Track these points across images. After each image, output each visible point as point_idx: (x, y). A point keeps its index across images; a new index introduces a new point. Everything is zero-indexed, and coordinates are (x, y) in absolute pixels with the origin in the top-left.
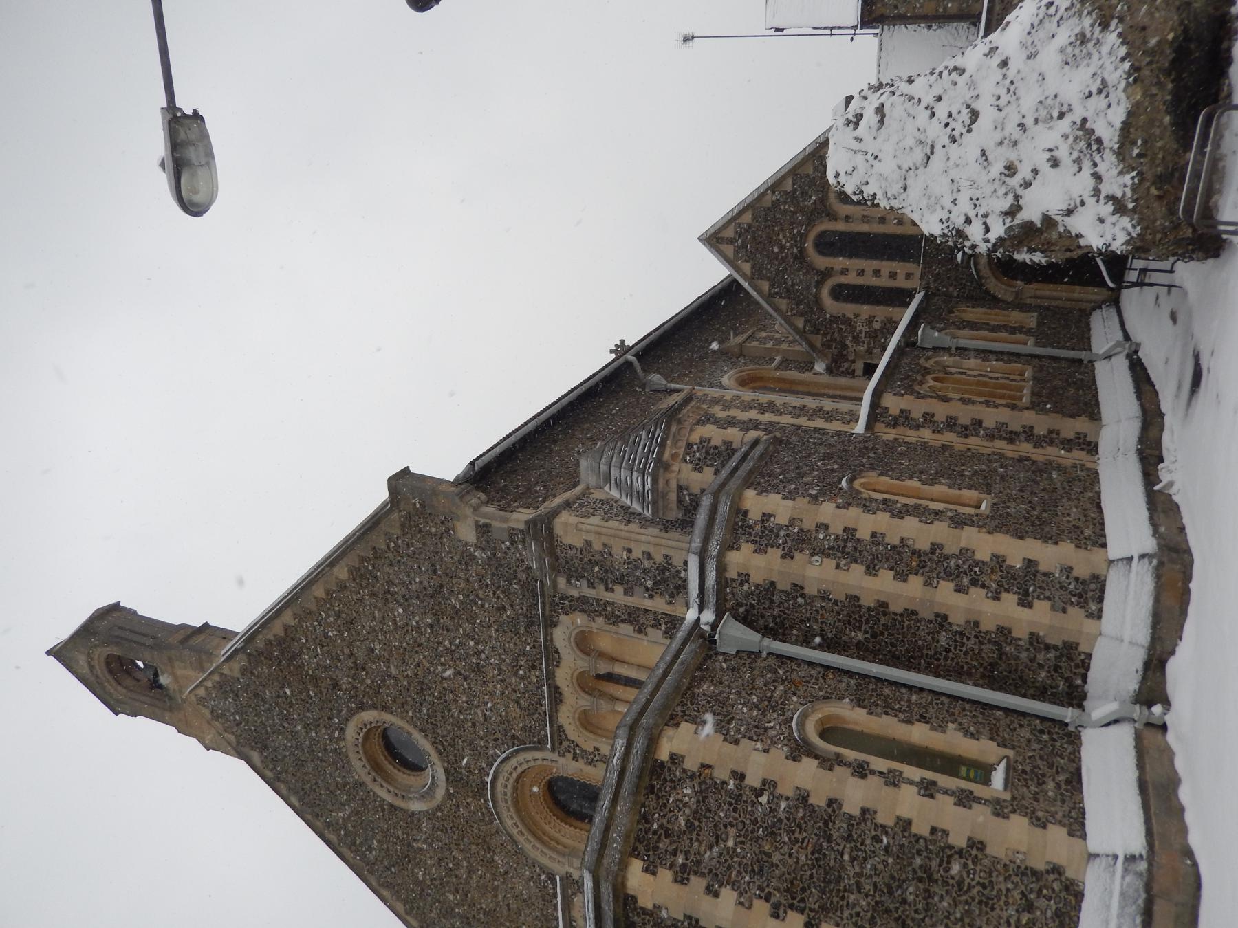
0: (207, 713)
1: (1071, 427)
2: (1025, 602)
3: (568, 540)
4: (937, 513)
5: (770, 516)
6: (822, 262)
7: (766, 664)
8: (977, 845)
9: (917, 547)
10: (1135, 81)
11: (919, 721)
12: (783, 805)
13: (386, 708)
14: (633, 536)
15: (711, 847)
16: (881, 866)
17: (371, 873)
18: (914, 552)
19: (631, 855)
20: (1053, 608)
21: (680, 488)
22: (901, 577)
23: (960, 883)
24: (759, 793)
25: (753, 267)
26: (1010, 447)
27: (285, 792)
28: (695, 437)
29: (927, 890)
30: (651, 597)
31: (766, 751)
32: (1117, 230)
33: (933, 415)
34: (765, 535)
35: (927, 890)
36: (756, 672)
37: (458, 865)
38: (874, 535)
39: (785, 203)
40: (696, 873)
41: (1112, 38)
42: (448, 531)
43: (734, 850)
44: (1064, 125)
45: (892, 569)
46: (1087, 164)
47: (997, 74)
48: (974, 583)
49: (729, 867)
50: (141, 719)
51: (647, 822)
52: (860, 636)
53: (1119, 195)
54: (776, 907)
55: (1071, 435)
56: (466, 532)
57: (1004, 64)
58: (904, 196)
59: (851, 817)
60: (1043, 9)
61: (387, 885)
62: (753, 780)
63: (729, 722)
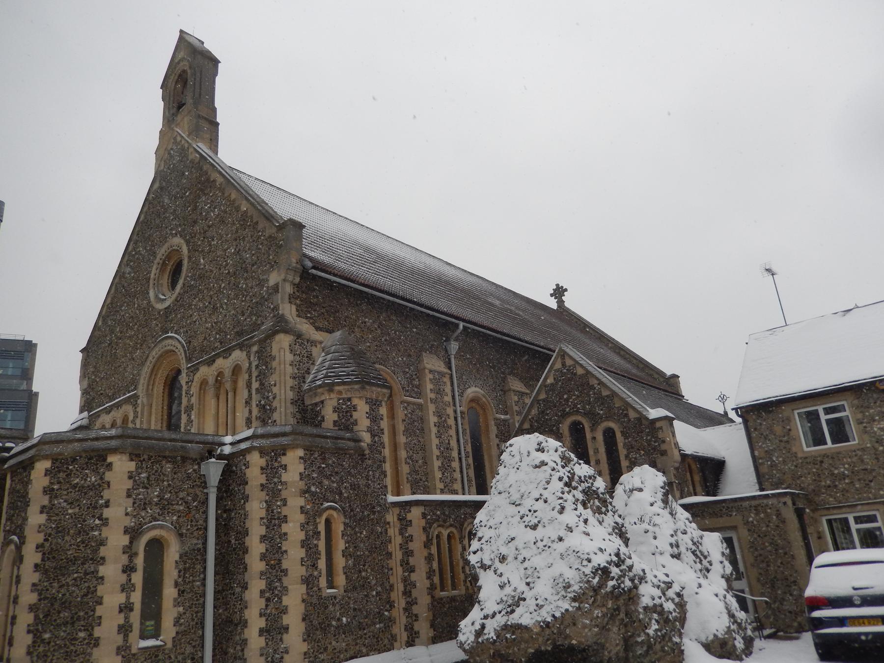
0: (170, 147)
1: (423, 627)
2: (262, 632)
3: (274, 345)
4: (314, 566)
5: (285, 469)
6: (565, 428)
7: (199, 493)
8: (96, 643)
9: (283, 561)
10: (541, 626)
11: (179, 590)
12: (96, 533)
13: (189, 257)
14: (283, 384)
15: (65, 501)
16: (75, 595)
17: (120, 278)
18: (280, 560)
19: (53, 459)
20: (261, 649)
21: (322, 402)
22: (263, 557)
23: (75, 639)
24: (100, 518)
25: (552, 384)
26: (400, 594)
27: (145, 209)
28: (355, 401)
29: (67, 623)
30: (257, 405)
31: (127, 514)
32: (468, 634)
33: (411, 541)
34: (273, 470)
35: (67, 623)
36: (190, 490)
37: (132, 329)
38: (285, 534)
39: (594, 394)
40: (51, 497)
41: (566, 605)
42: (272, 266)
43: (67, 514)
44: (522, 587)
45: (267, 550)
46: (500, 607)
47: (555, 537)
48: (268, 600)
49: (57, 515)
50: (161, 104)
51: (72, 462)
52: (233, 541)
53: (485, 632)
55: (416, 628)
56: (274, 278)
57: (561, 539)
58: (496, 493)
59: (97, 572)
60: (586, 556)
61: (116, 289)
62: (107, 513)
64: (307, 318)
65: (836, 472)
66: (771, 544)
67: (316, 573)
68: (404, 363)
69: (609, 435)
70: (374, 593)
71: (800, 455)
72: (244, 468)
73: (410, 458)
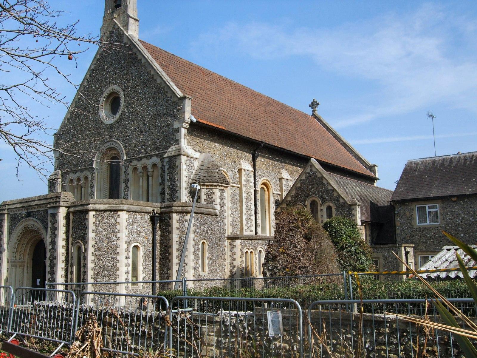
0: (111, 29)
13: (125, 100)
25: (304, 180)
31: (126, 236)
36: (147, 227)
39: (325, 188)
54: (94, 246)
62: (119, 235)
63: (131, 225)
64: (191, 146)
65: (428, 236)
66: (392, 266)
67: (198, 265)
68: (232, 166)
69: (329, 208)
70: (219, 275)
71: (415, 227)
72: (168, 219)
73: (232, 214)
